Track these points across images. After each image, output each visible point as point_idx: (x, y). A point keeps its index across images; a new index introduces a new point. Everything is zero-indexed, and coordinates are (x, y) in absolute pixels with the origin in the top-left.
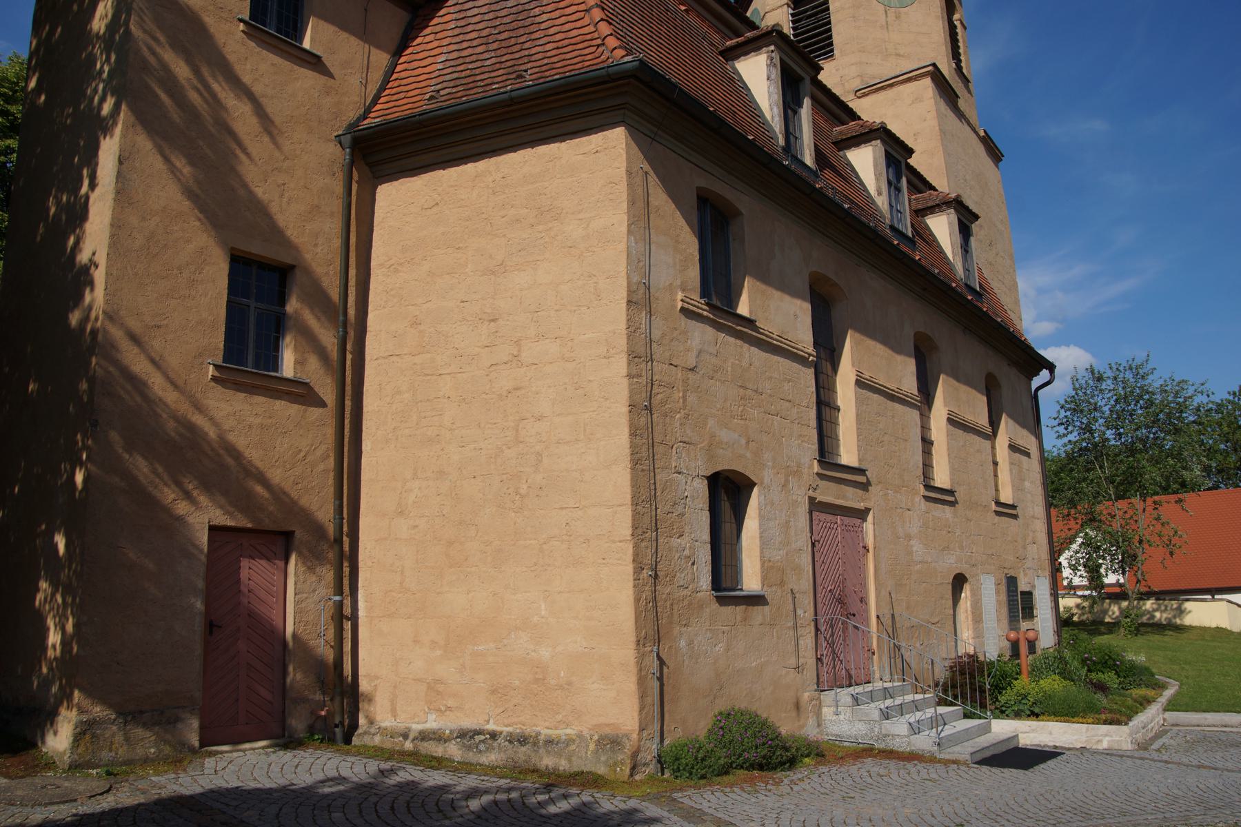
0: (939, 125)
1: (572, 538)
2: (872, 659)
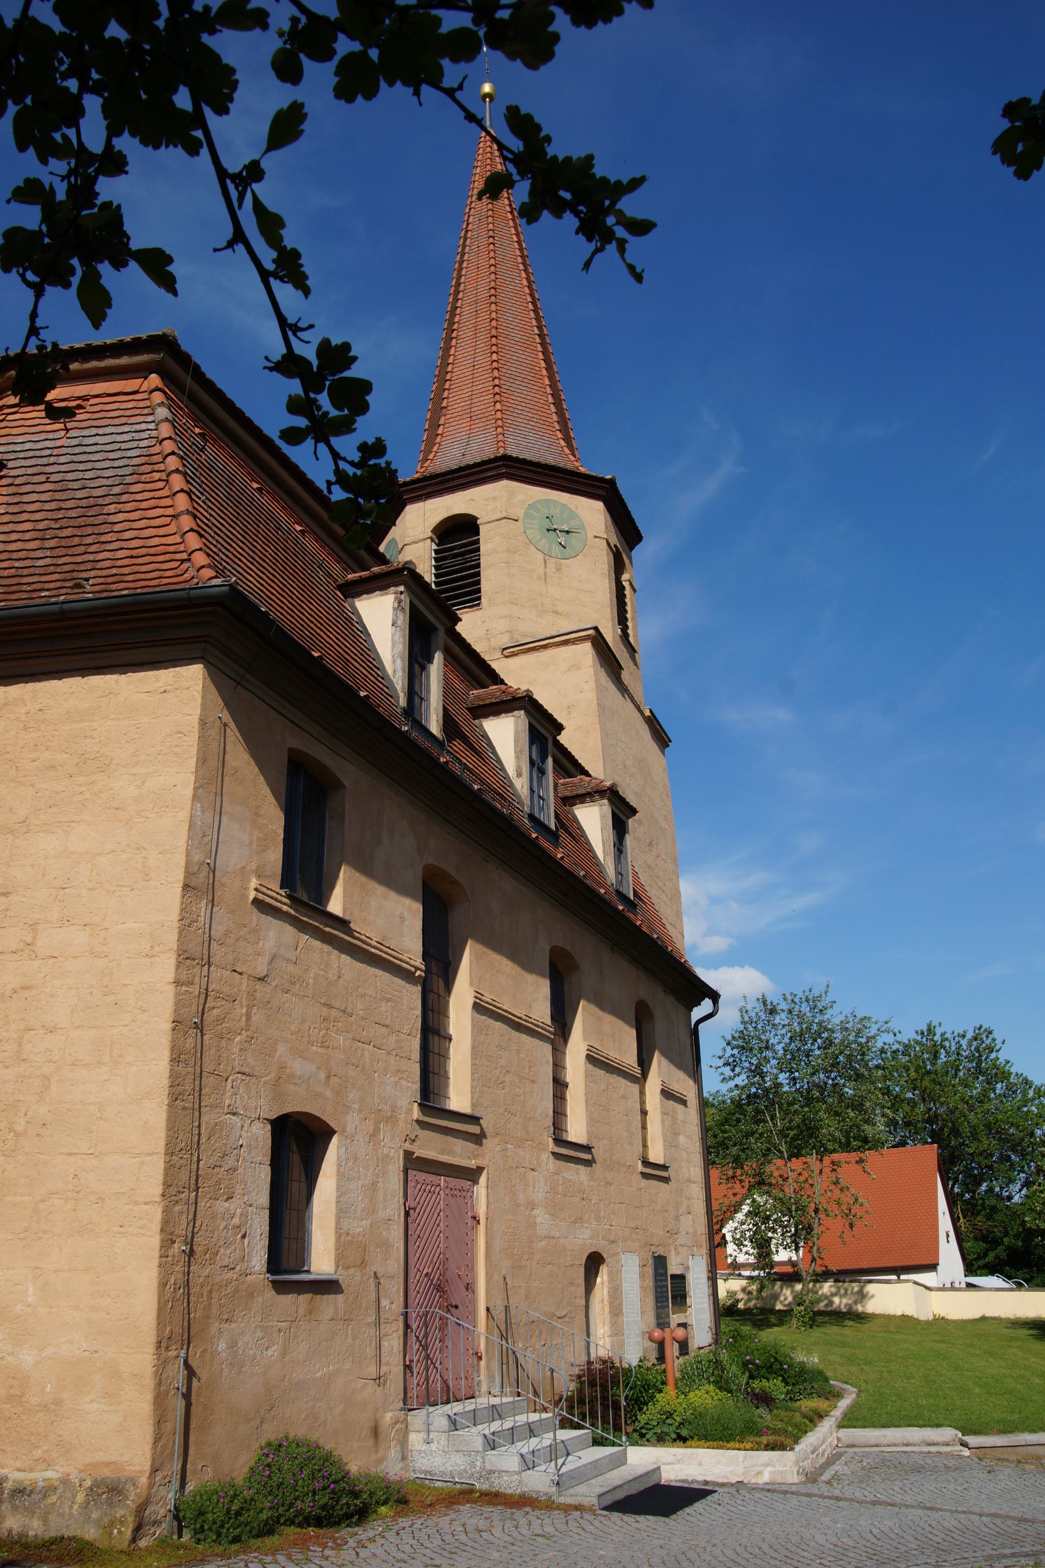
0: (598, 699)
1: (80, 1196)
2: (478, 1365)
